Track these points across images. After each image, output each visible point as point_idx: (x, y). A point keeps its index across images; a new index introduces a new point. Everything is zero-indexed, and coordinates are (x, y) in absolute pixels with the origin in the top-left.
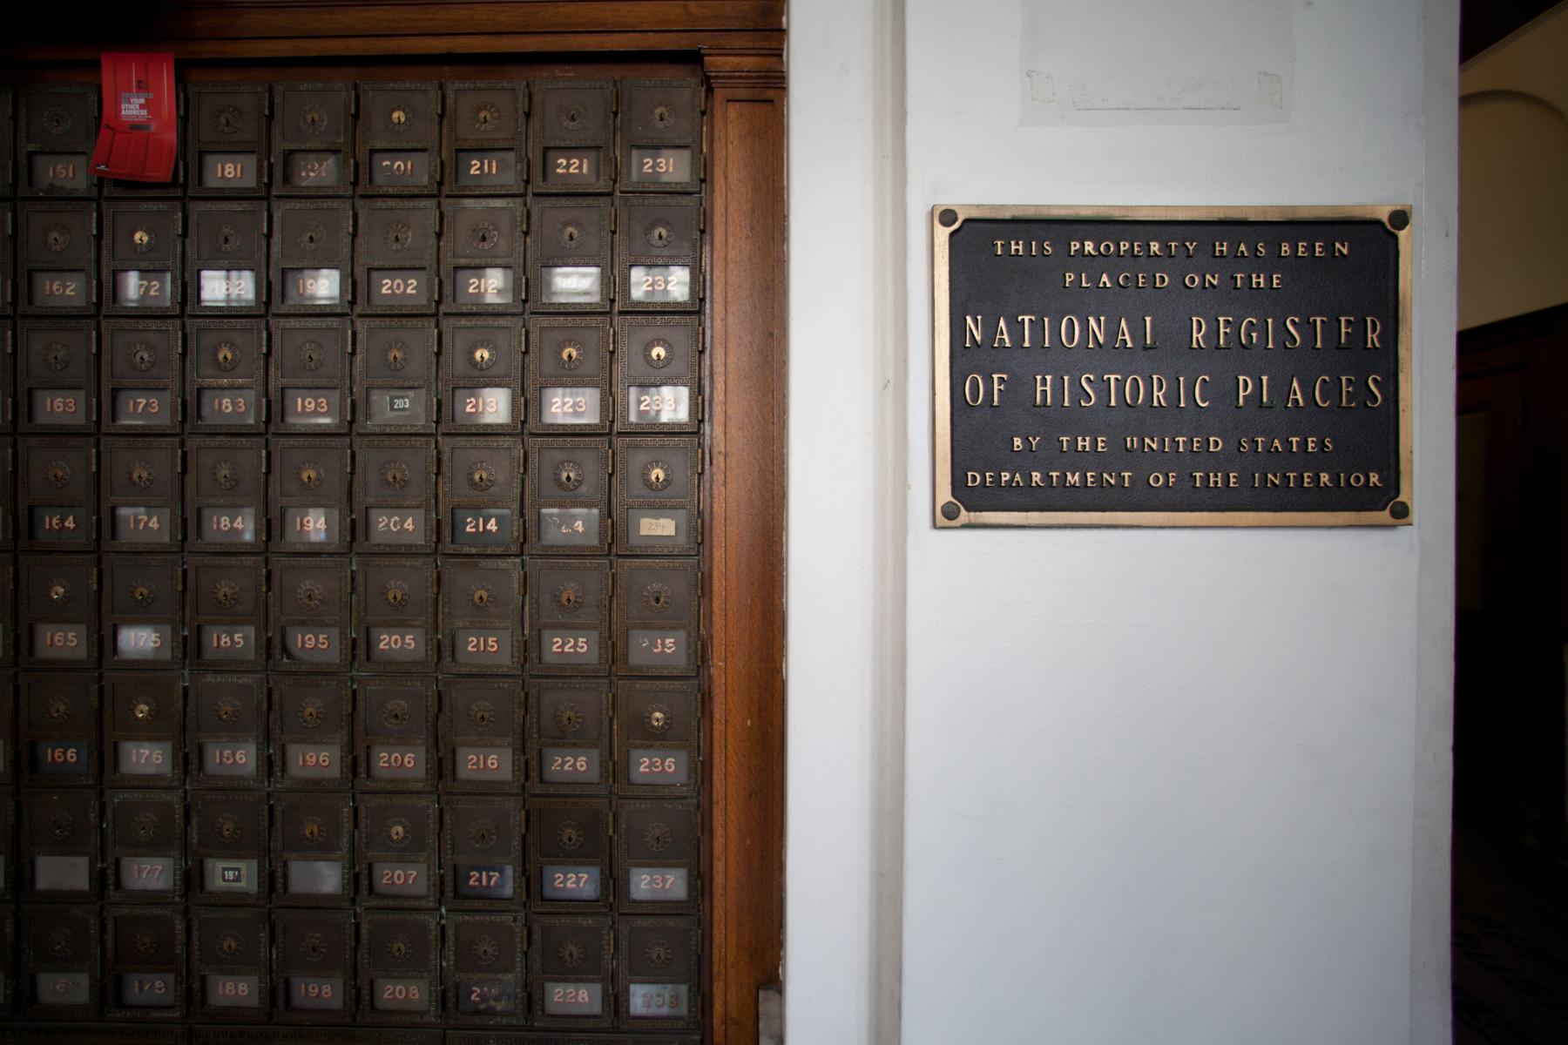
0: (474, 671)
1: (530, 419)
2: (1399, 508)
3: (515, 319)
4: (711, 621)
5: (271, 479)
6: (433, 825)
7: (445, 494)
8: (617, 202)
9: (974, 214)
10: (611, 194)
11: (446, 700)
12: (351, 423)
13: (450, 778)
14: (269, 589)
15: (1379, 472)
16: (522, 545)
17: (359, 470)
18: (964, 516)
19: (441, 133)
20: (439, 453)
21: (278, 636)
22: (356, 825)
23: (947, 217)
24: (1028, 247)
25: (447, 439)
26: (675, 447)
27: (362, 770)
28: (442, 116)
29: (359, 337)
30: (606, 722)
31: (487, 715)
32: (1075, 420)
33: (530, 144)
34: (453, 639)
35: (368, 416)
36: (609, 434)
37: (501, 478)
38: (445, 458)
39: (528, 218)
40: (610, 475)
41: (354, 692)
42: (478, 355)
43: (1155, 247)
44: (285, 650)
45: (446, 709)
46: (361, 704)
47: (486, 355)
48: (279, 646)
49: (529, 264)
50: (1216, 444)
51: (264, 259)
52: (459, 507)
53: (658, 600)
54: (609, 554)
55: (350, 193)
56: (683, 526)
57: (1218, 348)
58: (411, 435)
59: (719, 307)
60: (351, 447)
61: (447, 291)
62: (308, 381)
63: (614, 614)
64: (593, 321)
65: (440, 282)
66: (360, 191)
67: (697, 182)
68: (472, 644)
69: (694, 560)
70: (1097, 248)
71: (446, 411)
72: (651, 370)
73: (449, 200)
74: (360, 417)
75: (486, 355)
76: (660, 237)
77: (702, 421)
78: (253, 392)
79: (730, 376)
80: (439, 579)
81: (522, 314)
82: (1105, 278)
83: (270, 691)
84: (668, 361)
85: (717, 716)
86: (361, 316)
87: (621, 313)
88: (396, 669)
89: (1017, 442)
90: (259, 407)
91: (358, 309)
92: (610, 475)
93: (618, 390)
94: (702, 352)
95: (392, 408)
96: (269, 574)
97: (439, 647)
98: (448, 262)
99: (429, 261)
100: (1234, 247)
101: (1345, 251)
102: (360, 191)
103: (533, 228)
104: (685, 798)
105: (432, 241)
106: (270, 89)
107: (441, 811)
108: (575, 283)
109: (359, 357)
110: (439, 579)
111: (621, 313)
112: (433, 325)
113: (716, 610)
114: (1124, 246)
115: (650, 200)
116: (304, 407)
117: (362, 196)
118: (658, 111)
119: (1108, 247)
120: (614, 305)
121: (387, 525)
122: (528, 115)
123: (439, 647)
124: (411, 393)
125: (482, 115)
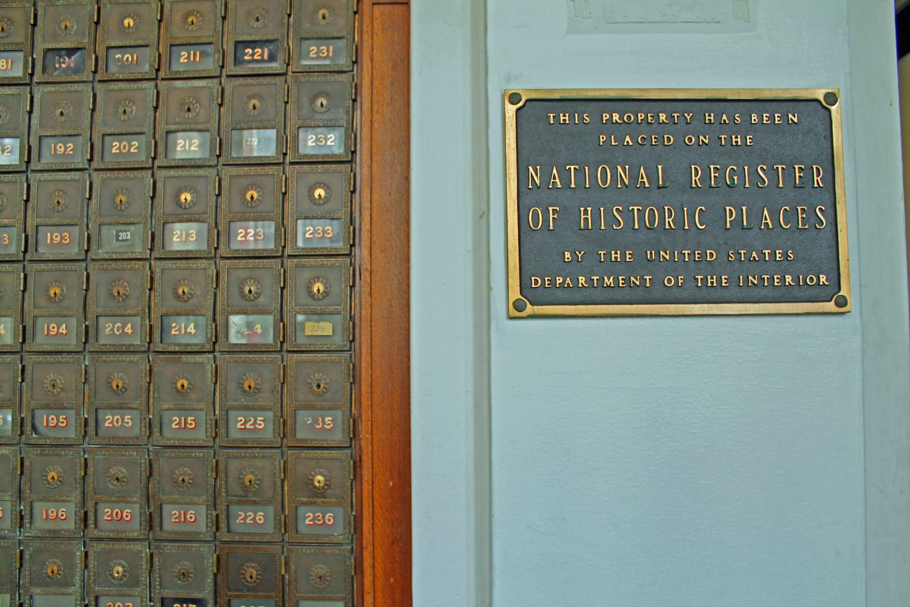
0: (177, 443)
1: (222, 246)
2: (841, 301)
3: (211, 170)
4: (360, 402)
5: (27, 295)
6: (145, 566)
7: (156, 304)
8: (289, 79)
9: (534, 96)
10: (285, 74)
11: (155, 466)
12: (87, 251)
13: (158, 529)
14: (23, 380)
15: (827, 275)
16: (214, 343)
17: (92, 287)
18: (530, 309)
19: (159, 33)
20: (152, 273)
21: (30, 417)
22: (86, 566)
23: (514, 98)
24: (572, 117)
25: (158, 263)
26: (332, 266)
27: (91, 521)
28: (160, 21)
29: (95, 186)
30: (279, 484)
31: (186, 479)
32: (609, 240)
33: (225, 39)
34: (161, 418)
35: (99, 246)
36: (282, 257)
37: (198, 292)
38: (157, 277)
39: (223, 93)
40: (282, 289)
41: (86, 460)
42: (183, 197)
43: (663, 117)
44: (34, 429)
45: (155, 474)
46: (91, 469)
47: (189, 198)
48: (30, 425)
49: (222, 128)
50: (711, 255)
51: (26, 130)
52: (167, 315)
53: (319, 386)
54: (281, 351)
55: (91, 79)
56: (339, 327)
57: (711, 187)
58: (131, 260)
59: (366, 157)
60: (86, 270)
61: (161, 149)
62: (56, 220)
63: (285, 398)
64: (270, 170)
65: (156, 143)
66: (98, 77)
67: (350, 64)
68: (175, 421)
69: (347, 354)
70: (621, 118)
71: (158, 241)
72: (314, 207)
73: (164, 82)
74: (94, 246)
75: (189, 198)
76: (322, 105)
77: (353, 245)
78: (15, 229)
79: (375, 210)
80: (151, 371)
81: (217, 166)
82: (628, 139)
83: (22, 459)
84: (327, 200)
85: (365, 478)
86: (96, 170)
87: (291, 163)
88: (119, 443)
89: (567, 255)
90: (19, 240)
91: (95, 165)
92: (282, 289)
93: (288, 222)
94: (353, 192)
95: (117, 240)
96: (23, 368)
97: (150, 425)
98: (162, 128)
99: (148, 129)
100: (718, 116)
101: (796, 120)
102: (98, 77)
103: (226, 101)
104: (340, 544)
105: (151, 112)
106: (35, 5)
107: (152, 555)
108: (259, 143)
109: (94, 200)
110: (151, 371)
111: (291, 163)
112: (150, 175)
113: (364, 393)
114: (641, 117)
115: (314, 78)
116: (52, 239)
117: (100, 81)
118: (321, 12)
119: (629, 117)
120: (288, 157)
121: (112, 330)
122: (224, 18)
123: (150, 425)
124: (132, 228)
125: (190, 20)
